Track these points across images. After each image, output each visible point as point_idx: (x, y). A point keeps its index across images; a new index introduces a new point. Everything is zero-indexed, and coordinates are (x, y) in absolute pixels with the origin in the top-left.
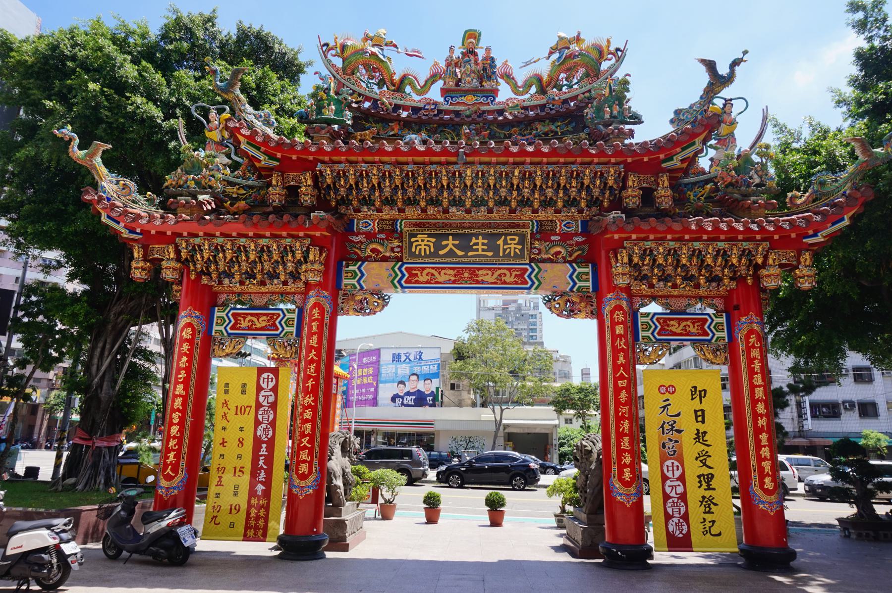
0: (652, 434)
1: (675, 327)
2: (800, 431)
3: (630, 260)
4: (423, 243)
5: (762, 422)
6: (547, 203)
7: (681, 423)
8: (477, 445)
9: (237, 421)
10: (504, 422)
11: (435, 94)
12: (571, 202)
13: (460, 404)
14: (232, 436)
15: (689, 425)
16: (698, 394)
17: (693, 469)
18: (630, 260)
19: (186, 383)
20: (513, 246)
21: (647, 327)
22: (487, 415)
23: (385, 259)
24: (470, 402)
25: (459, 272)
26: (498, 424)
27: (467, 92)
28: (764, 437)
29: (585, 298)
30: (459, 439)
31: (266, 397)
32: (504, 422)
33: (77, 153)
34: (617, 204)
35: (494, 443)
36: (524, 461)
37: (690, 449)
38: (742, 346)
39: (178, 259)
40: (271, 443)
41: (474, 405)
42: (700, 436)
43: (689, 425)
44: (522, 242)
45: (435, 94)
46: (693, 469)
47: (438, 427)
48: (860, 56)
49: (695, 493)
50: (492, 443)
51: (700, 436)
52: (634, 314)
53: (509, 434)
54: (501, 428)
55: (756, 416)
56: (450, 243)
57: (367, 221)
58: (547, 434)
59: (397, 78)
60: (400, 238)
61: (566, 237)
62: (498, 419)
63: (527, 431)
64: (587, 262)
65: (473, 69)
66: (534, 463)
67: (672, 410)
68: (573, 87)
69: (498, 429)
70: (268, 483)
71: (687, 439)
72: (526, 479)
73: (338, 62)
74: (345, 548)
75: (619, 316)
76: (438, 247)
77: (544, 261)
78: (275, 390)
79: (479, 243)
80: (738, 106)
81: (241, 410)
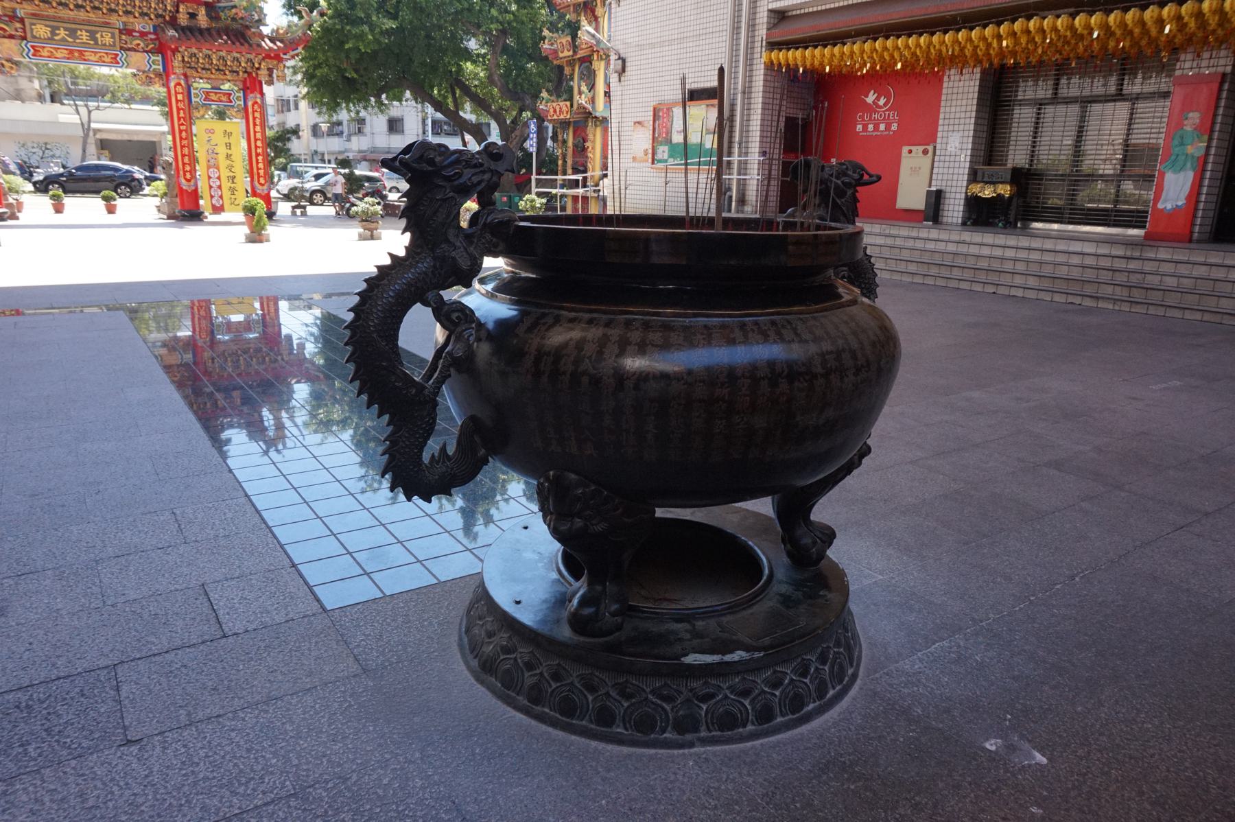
0: (201, 155)
1: (213, 97)
3: (183, 61)
4: (41, 30)
5: (259, 151)
7: (218, 149)
8: (58, 153)
10: (93, 125)
12: (143, 14)
15: (222, 150)
17: (225, 173)
18: (183, 61)
20: (108, 39)
21: (197, 96)
22: (66, 115)
23: (11, 37)
24: (34, 94)
25: (71, 52)
26: (86, 129)
28: (260, 158)
29: (158, 75)
30: (30, 145)
32: (93, 125)
34: (173, 23)
35: (84, 151)
36: (128, 171)
37: (223, 163)
38: (250, 110)
41: (41, 98)
42: (228, 157)
43: (222, 150)
44: (113, 37)
49: (226, 185)
50: (81, 152)
51: (228, 157)
52: (189, 87)
53: (101, 141)
54: (91, 133)
55: (256, 147)
58: (154, 143)
60: (22, 21)
61: (143, 35)
62: (85, 119)
63: (126, 137)
64: (158, 53)
66: (139, 173)
67: (213, 142)
69: (86, 136)
71: (222, 159)
72: (132, 187)
74: (17, 218)
75: (179, 89)
76: (53, 33)
77: (129, 49)
79: (84, 36)
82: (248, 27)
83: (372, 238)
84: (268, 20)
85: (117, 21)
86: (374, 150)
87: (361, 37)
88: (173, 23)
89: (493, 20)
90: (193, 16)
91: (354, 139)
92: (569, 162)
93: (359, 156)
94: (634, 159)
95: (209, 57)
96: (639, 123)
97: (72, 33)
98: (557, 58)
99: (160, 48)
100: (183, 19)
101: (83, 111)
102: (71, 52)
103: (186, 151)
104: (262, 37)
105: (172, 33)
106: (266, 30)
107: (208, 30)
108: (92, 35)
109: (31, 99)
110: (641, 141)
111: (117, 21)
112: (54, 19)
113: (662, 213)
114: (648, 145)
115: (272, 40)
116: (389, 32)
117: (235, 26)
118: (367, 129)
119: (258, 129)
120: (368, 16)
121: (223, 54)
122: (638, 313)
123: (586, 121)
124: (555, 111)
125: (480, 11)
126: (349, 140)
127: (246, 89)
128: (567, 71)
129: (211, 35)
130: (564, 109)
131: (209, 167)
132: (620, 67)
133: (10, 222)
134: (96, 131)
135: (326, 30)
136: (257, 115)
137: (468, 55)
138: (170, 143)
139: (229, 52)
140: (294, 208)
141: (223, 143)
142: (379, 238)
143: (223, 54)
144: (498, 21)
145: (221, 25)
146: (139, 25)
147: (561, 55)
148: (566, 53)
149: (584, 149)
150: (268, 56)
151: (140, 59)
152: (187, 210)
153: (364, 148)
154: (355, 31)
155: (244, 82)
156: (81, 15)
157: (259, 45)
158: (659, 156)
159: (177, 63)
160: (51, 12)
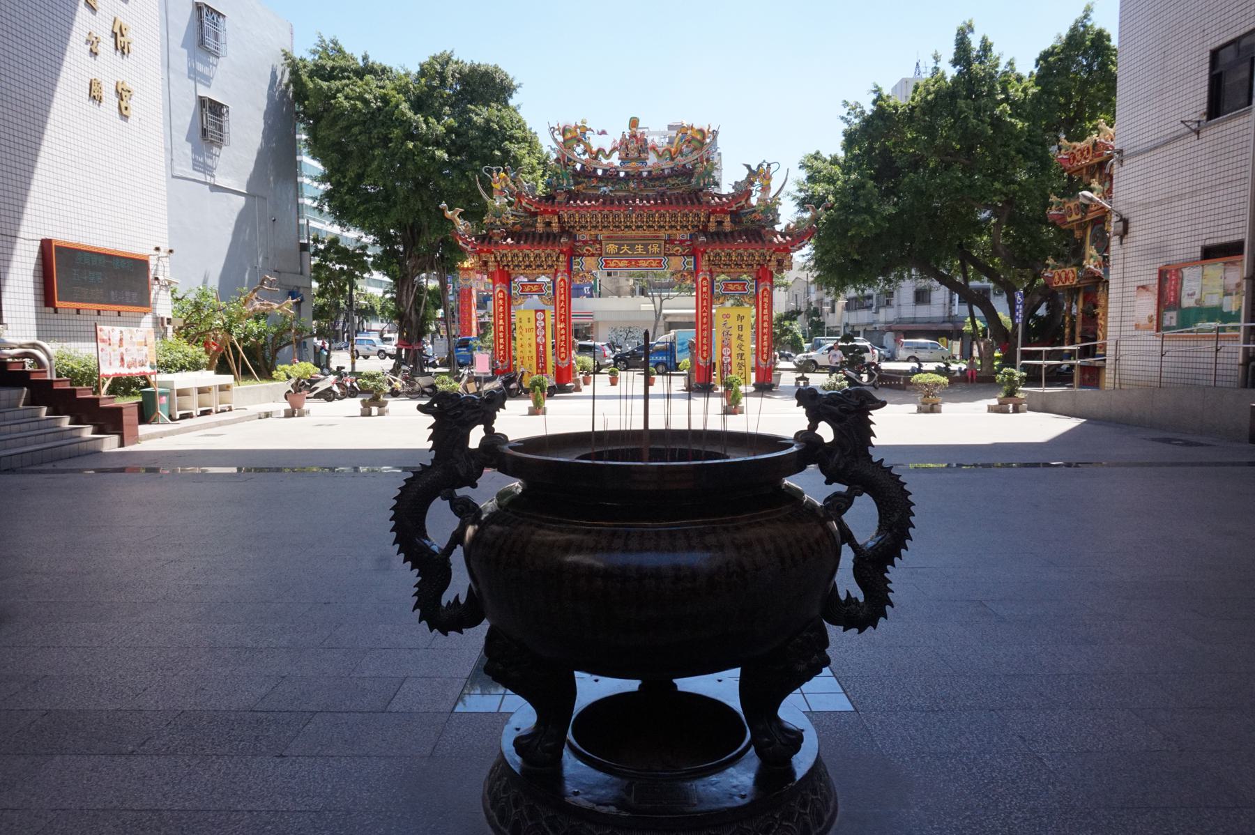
2: (950, 316)
4: (612, 248)
6: (671, 227)
9: (527, 335)
10: (664, 311)
11: (615, 160)
12: (683, 227)
13: (618, 293)
14: (526, 342)
16: (740, 318)
17: (735, 351)
19: (504, 319)
20: (656, 249)
22: (646, 305)
23: (593, 255)
24: (628, 289)
25: (630, 261)
26: (658, 314)
27: (632, 160)
29: (691, 273)
31: (540, 324)
32: (664, 311)
33: (449, 214)
34: (705, 231)
37: (735, 342)
39: (496, 261)
40: (544, 345)
41: (633, 293)
42: (740, 337)
45: (615, 160)
46: (735, 351)
47: (597, 318)
48: (846, 134)
51: (740, 337)
56: (625, 248)
57: (584, 235)
59: (595, 149)
60: (600, 243)
61: (682, 242)
65: (635, 144)
68: (687, 160)
70: (545, 362)
73: (560, 139)
76: (619, 249)
78: (544, 320)
80: (773, 167)
81: (528, 330)
82: (764, 227)
83: (932, 411)
84: (781, 219)
85: (663, 234)
86: (900, 321)
87: (862, 224)
88: (705, 231)
89: (996, 192)
90: (720, 223)
91: (882, 311)
92: (1078, 329)
93: (884, 327)
94: (1137, 327)
95: (730, 255)
96: (1143, 287)
97: (632, 247)
98: (1065, 223)
99: (694, 253)
100: (712, 227)
101: (657, 300)
102: (630, 261)
103: (705, 333)
104: (775, 233)
105: (702, 239)
106: (778, 228)
107: (732, 233)
108: (645, 246)
109: (626, 294)
110: (1146, 306)
111: (663, 234)
112: (621, 238)
113: (745, 430)
114: (1153, 311)
115: (783, 235)
116: (890, 219)
117: (754, 227)
118: (894, 301)
119: (766, 312)
120: (870, 206)
121: (741, 251)
122: (606, 526)
123: (1097, 286)
124: (1060, 277)
125: (982, 186)
126: (877, 312)
127: (758, 280)
128: (1078, 234)
129: (730, 239)
130: (1071, 275)
131: (723, 347)
132: (1120, 229)
133: (575, 394)
134: (666, 316)
135: (831, 221)
136: (766, 300)
137: (979, 228)
138: (753, 320)
139: (746, 249)
140: (797, 379)
141: (736, 324)
142: (939, 412)
143: (741, 251)
144: (1002, 193)
145: (742, 227)
146: (680, 235)
147: (1069, 219)
148: (1074, 217)
149: (1095, 316)
150: (778, 250)
151: (677, 263)
152: (700, 386)
153: (891, 319)
154: (858, 219)
155: (758, 272)
156: (640, 232)
157: (771, 241)
158: (1166, 323)
159: (704, 263)
160: (620, 233)
